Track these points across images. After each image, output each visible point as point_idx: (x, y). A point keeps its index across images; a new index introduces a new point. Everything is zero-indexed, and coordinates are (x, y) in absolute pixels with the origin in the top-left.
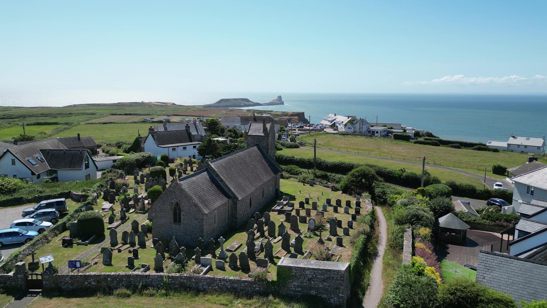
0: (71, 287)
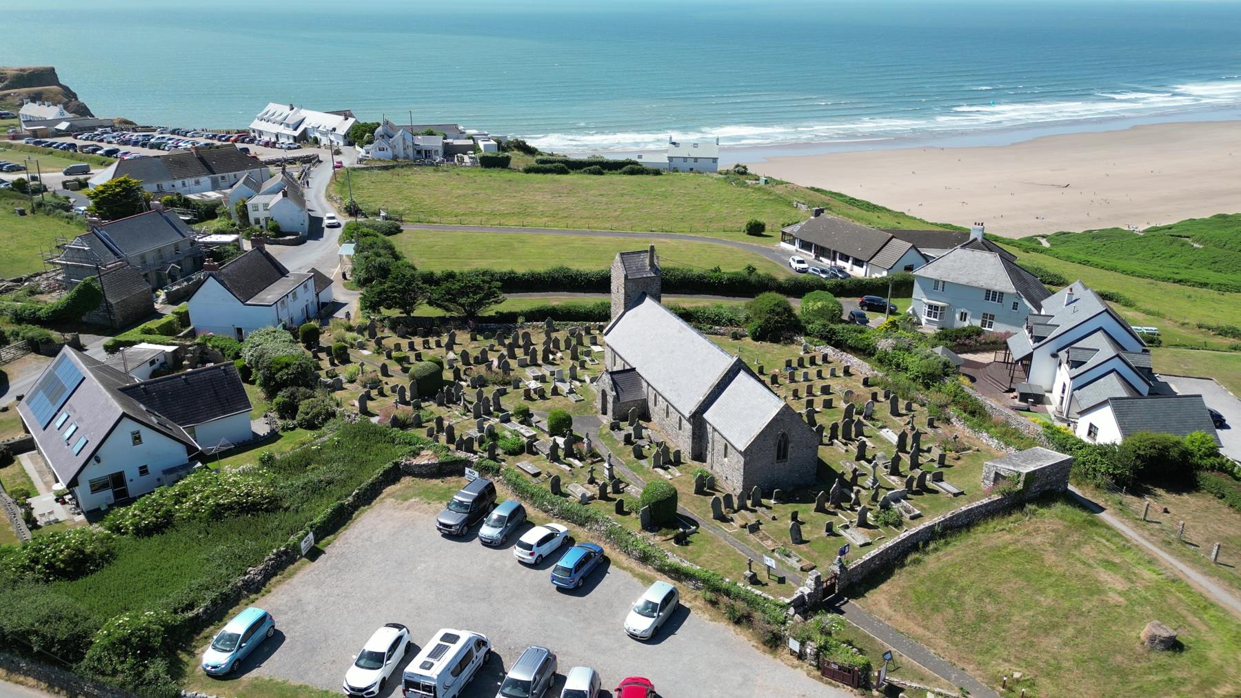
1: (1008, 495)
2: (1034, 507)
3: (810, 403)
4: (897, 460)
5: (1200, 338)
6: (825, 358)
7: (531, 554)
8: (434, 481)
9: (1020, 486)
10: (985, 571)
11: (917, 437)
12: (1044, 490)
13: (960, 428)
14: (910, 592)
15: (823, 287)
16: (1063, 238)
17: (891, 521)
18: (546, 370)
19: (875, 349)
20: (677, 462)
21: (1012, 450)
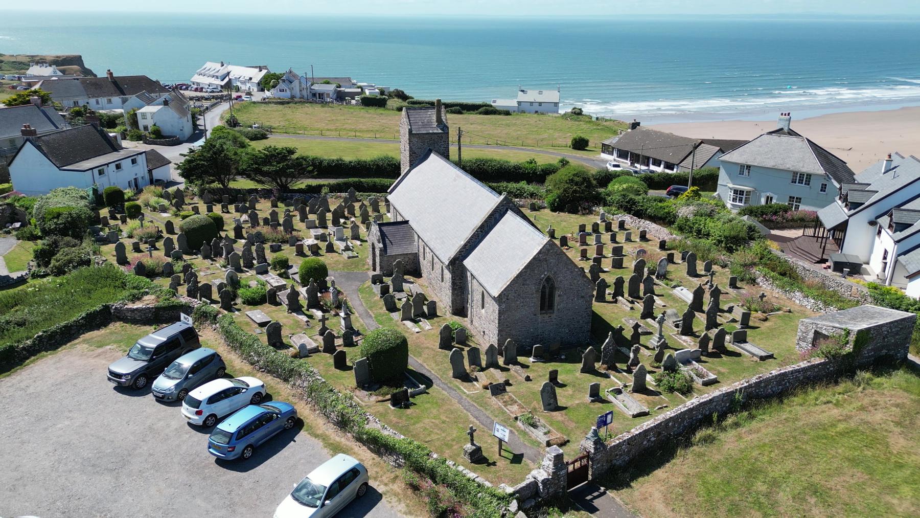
0: (627, 458)
1: (833, 358)
2: (868, 375)
3: (598, 261)
6: (622, 225)
7: (199, 413)
9: (849, 348)
10: (807, 459)
13: (769, 289)
14: (698, 486)
17: (676, 386)
19: (675, 217)
20: (432, 314)
21: (833, 309)
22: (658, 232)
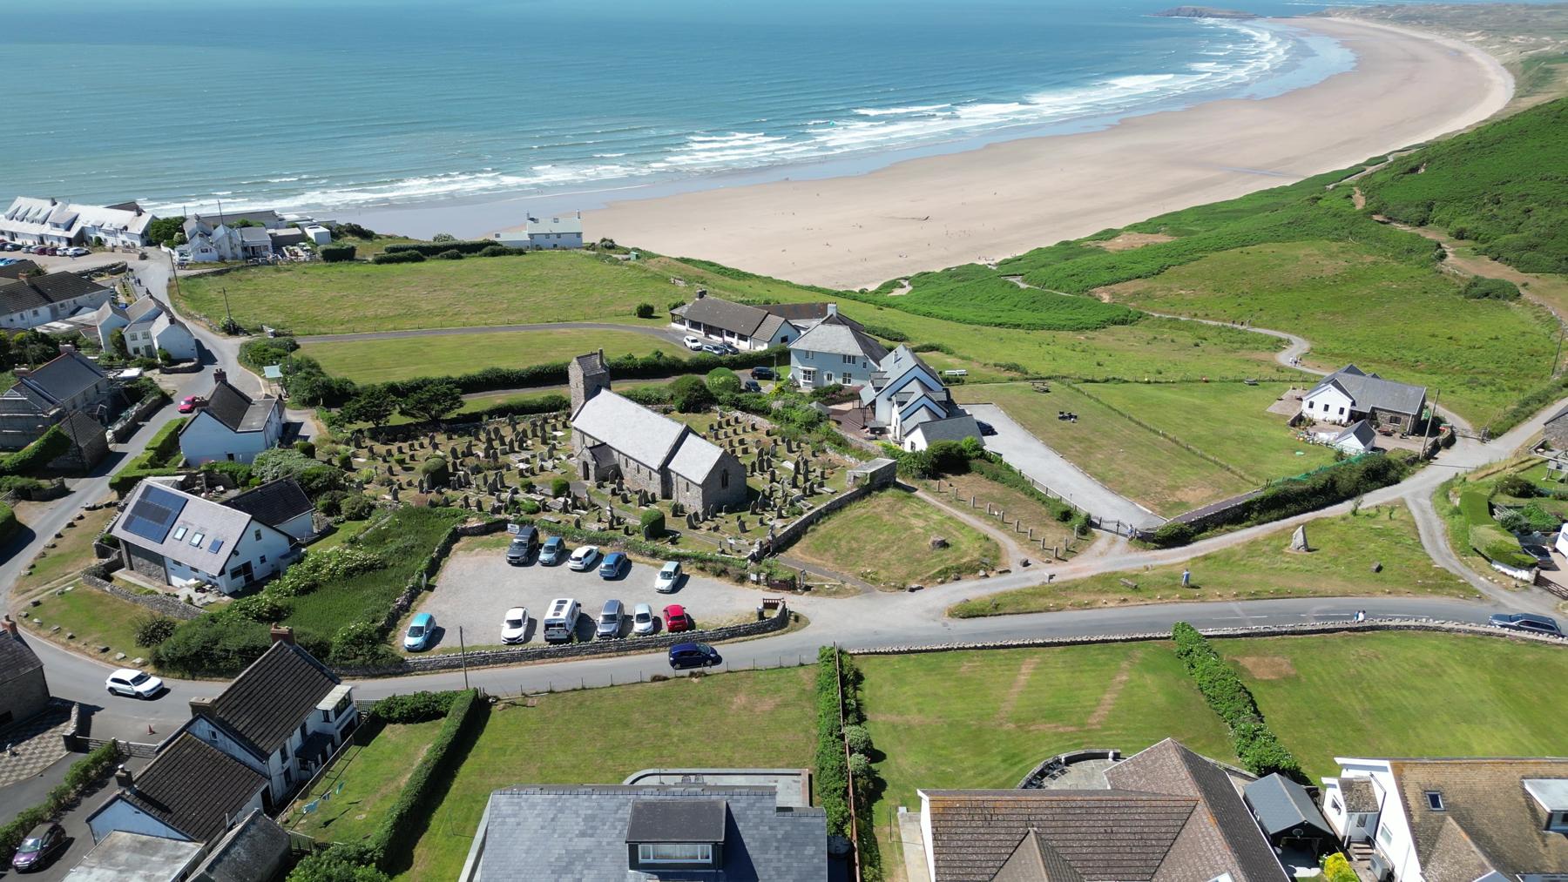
4: (795, 479)
5: (994, 374)
6: (736, 420)
8: (485, 537)
11: (806, 463)
12: (881, 482)
13: (832, 455)
15: (720, 364)
16: (923, 279)
18: (525, 455)
20: (654, 501)
22: (763, 423)
